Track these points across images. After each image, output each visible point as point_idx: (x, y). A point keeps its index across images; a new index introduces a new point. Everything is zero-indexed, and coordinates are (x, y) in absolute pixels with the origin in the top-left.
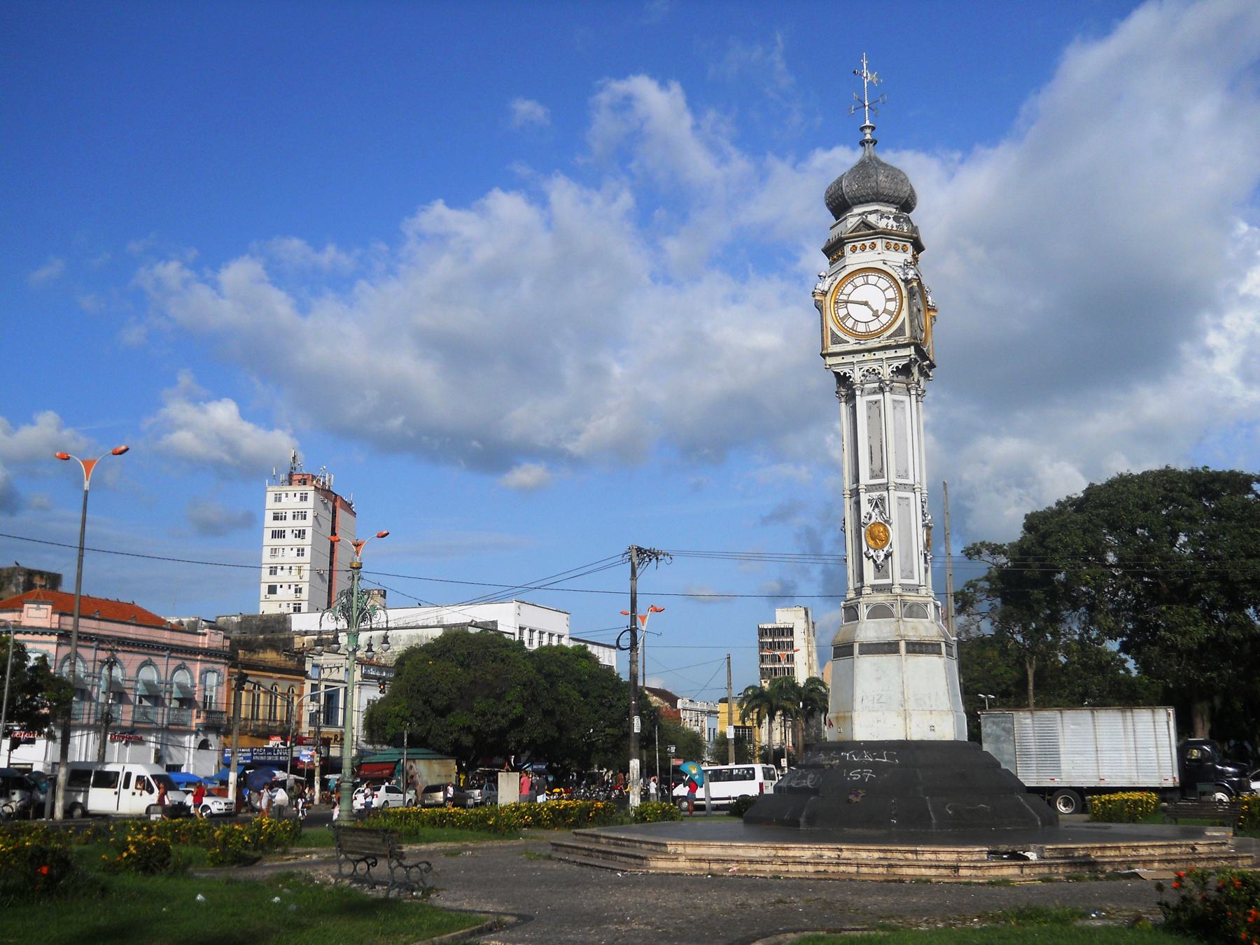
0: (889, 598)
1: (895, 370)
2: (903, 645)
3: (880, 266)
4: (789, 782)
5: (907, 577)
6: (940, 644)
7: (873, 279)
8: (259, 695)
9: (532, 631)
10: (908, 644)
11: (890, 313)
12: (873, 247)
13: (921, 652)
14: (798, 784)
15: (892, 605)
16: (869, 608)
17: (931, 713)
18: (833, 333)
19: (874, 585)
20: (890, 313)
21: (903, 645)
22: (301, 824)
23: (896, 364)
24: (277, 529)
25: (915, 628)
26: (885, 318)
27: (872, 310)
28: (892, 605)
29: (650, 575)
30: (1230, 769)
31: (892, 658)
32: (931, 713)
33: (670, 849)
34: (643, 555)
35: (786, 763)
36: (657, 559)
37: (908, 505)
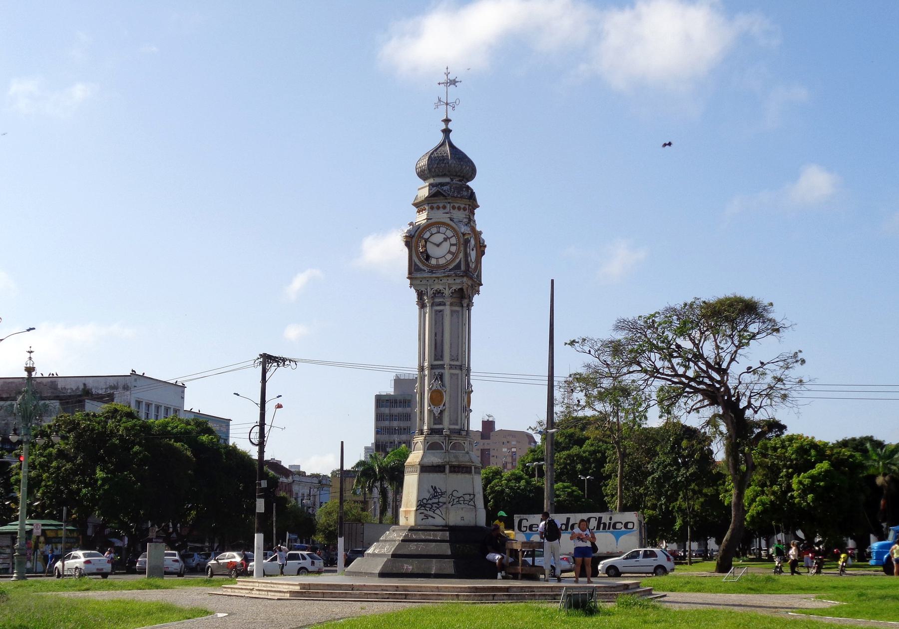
0: (441, 438)
1: (453, 291)
2: (447, 467)
3: (448, 221)
4: (374, 550)
5: (454, 424)
6: (471, 467)
7: (442, 229)
9: (158, 407)
11: (453, 254)
12: (444, 207)
13: (458, 472)
14: (379, 552)
15: (464, 443)
16: (429, 444)
17: (462, 510)
18: (416, 265)
19: (433, 429)
20: (453, 254)
21: (447, 467)
22: (766, 483)
23: (454, 288)
25: (456, 457)
26: (449, 257)
27: (443, 242)
29: (276, 374)
30: (36, 504)
31: (441, 475)
32: (462, 510)
33: (299, 587)
34: (267, 360)
35: (258, 505)
36: (284, 364)
37: (457, 378)
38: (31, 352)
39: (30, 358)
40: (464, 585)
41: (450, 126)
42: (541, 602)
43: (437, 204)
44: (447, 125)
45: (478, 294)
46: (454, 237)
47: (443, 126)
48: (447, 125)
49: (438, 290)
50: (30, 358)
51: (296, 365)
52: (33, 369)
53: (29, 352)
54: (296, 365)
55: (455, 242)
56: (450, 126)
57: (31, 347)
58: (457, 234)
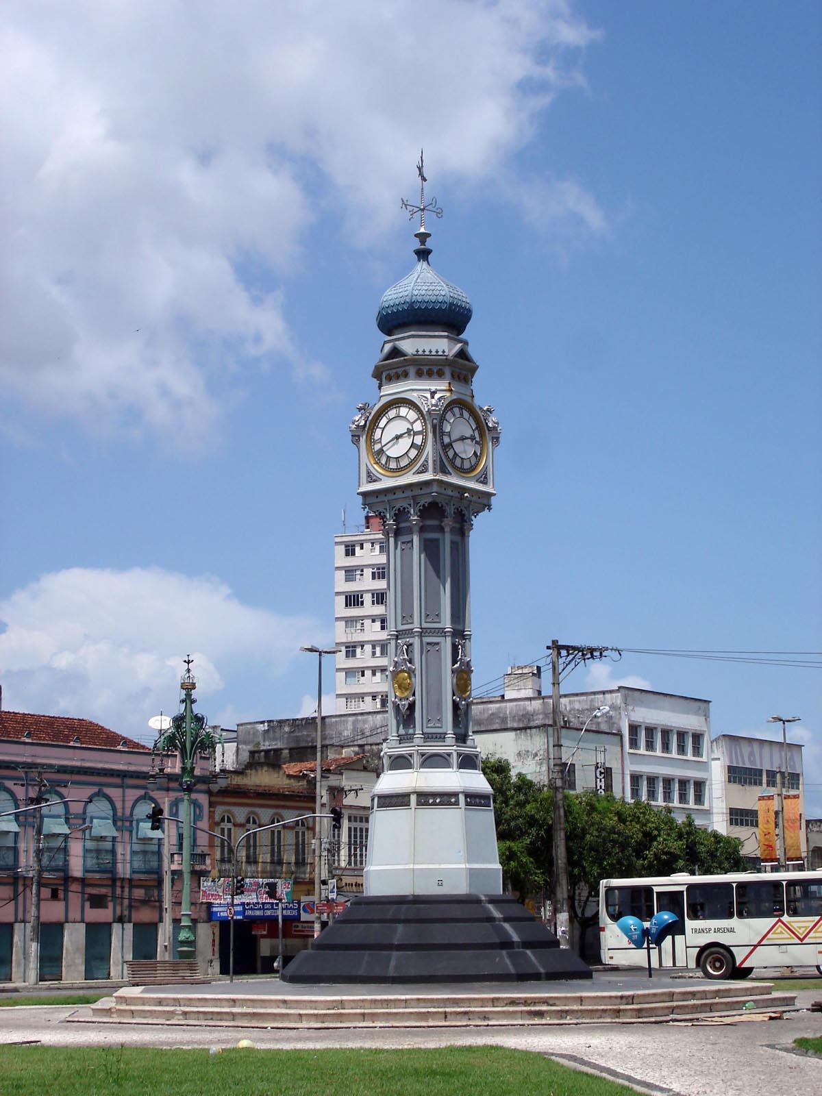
1: (421, 508)
8: (229, 830)
10: (467, 795)
15: (411, 756)
21: (413, 798)
24: (352, 594)
26: (413, 453)
28: (411, 756)
38: (189, 662)
39: (189, 671)
40: (574, 992)
41: (429, 244)
42: (19, 1019)
43: (404, 369)
44: (423, 243)
45: (489, 509)
46: (419, 421)
47: (417, 245)
48: (423, 243)
49: (402, 508)
50: (189, 671)
51: (620, 655)
52: (193, 686)
53: (185, 661)
54: (620, 655)
55: (420, 429)
56: (429, 244)
57: (188, 656)
58: (422, 415)
